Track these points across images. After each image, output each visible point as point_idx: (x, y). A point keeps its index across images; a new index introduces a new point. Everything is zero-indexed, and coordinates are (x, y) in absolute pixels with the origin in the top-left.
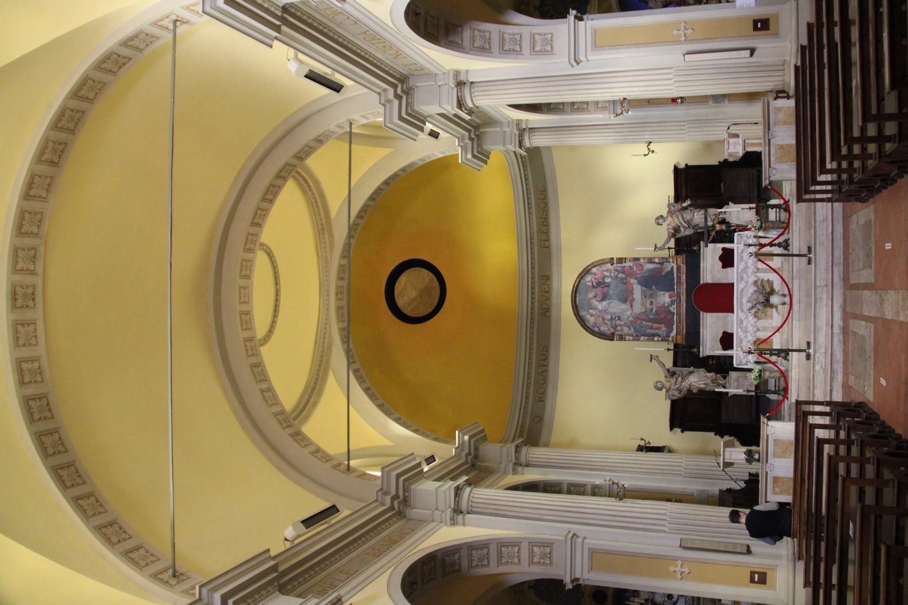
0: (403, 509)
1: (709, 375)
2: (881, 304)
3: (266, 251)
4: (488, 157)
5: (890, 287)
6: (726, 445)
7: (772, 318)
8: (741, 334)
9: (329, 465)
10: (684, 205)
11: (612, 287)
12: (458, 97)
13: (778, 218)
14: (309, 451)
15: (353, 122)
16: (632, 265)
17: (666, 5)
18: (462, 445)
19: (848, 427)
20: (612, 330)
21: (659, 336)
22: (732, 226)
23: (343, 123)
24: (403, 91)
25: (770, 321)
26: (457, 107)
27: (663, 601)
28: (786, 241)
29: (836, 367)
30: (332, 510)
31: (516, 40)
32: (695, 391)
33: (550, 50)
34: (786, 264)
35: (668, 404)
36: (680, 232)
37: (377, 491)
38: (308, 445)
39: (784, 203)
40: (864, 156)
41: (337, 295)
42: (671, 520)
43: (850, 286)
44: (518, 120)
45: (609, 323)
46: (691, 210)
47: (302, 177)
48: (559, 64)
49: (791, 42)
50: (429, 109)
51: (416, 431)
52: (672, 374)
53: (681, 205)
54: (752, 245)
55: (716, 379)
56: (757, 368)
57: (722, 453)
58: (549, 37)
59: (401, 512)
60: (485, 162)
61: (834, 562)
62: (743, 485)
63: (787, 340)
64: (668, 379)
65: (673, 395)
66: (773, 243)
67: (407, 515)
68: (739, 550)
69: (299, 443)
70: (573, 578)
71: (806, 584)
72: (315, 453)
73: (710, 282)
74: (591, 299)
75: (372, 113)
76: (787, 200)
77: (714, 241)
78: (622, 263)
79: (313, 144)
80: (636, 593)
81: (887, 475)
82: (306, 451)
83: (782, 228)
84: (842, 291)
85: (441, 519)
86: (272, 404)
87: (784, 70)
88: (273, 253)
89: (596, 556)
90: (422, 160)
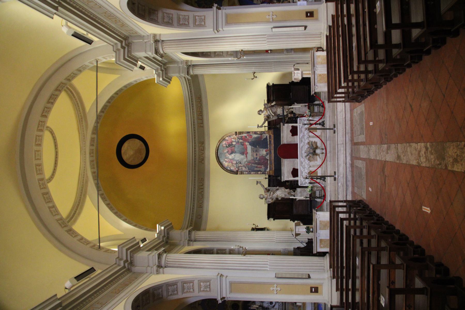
0: (130, 267)
1: (286, 190)
2: (369, 152)
3: (50, 131)
4: (171, 80)
5: (373, 144)
6: (296, 225)
7: (317, 161)
8: (302, 169)
9: (88, 246)
10: (272, 104)
11: (237, 146)
12: (155, 48)
13: (319, 111)
14: (77, 239)
15: (98, 61)
16: (246, 135)
17: (263, 3)
18: (160, 232)
19: (355, 212)
20: (237, 169)
21: (261, 171)
22: (296, 115)
23: (93, 61)
24: (126, 44)
25: (316, 162)
26: (155, 54)
27: (268, 306)
28: (323, 122)
29: (348, 183)
30: (92, 270)
31: (186, 19)
32: (280, 199)
33: (204, 24)
34: (323, 135)
35: (266, 206)
36: (270, 118)
37: (116, 259)
38: (76, 236)
39: (322, 103)
40: (359, 80)
41: (90, 154)
42: (270, 267)
43: (354, 144)
44: (187, 60)
45: (235, 166)
46: (276, 107)
47: (70, 90)
48: (208, 32)
49: (324, 24)
50: (141, 54)
51: (135, 226)
52: (267, 190)
53: (271, 104)
54: (306, 124)
55: (290, 192)
56: (310, 186)
57: (294, 229)
58: (203, 17)
59: (129, 269)
60: (169, 83)
61: (350, 278)
62: (305, 245)
63: (325, 171)
64: (266, 193)
65: (269, 201)
66: (317, 123)
67: (133, 270)
68: (304, 277)
69: (71, 235)
70: (221, 297)
71: (337, 290)
72: (80, 240)
73: (286, 143)
74: (225, 153)
75: (109, 56)
76: (323, 101)
77: (288, 122)
78: (241, 134)
79: (75, 72)
80: (254, 303)
81: (373, 233)
82: (75, 239)
83: (321, 115)
84: (350, 146)
85: (151, 271)
86: (55, 215)
87: (321, 37)
88: (53, 132)
89: (233, 285)
90: (136, 81)
